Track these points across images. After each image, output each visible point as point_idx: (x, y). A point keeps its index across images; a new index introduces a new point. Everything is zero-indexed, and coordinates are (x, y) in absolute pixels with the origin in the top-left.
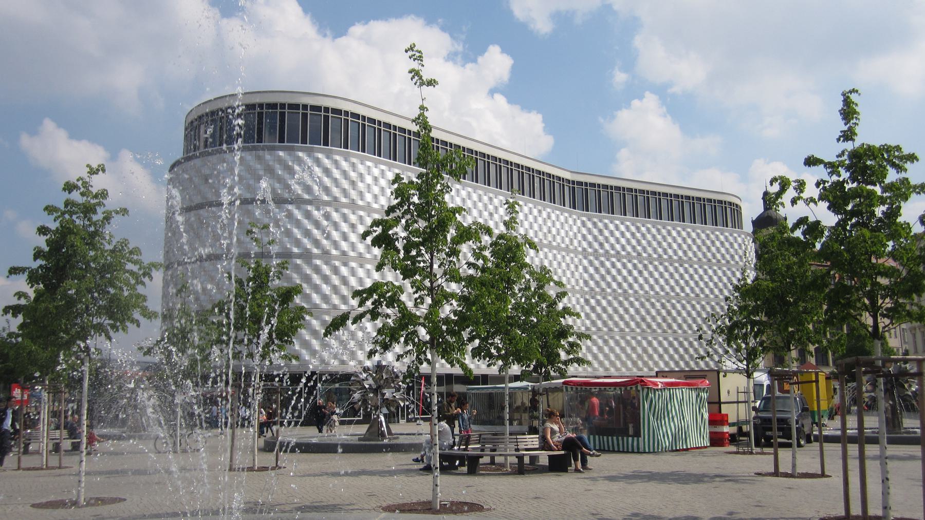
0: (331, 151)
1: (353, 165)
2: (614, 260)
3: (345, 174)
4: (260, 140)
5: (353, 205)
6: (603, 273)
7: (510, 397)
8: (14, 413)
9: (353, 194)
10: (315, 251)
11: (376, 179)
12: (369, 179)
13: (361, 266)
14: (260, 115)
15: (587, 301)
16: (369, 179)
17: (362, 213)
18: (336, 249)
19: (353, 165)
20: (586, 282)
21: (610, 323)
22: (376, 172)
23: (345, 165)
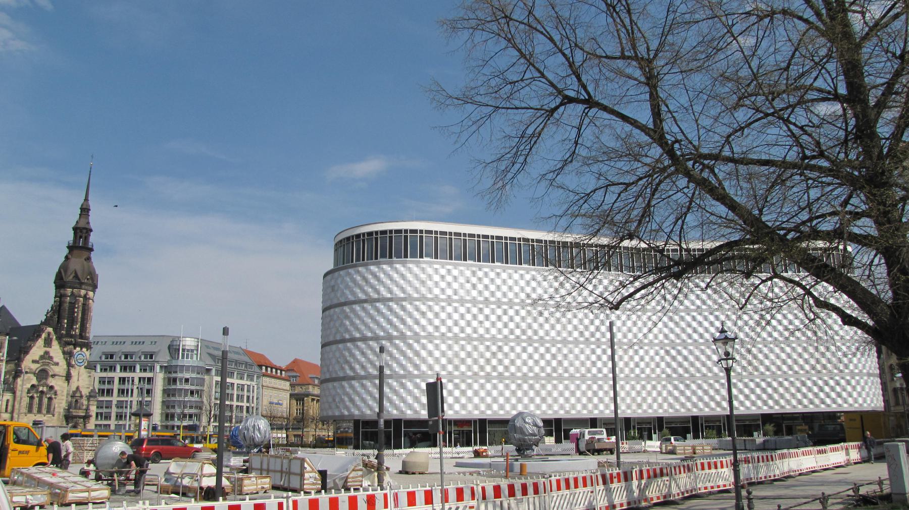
0: (406, 262)
1: (423, 270)
2: (695, 314)
3: (416, 277)
4: (406, 256)
5: (423, 299)
6: (684, 326)
7: (105, 425)
8: (192, 442)
9: (423, 290)
10: (409, 333)
11: (443, 277)
12: (436, 278)
13: (431, 342)
14: (436, 238)
15: (667, 352)
16: (436, 278)
17: (431, 303)
18: (796, 315)
19: (423, 270)
20: (666, 336)
21: (692, 369)
22: (443, 272)
23: (416, 269)
